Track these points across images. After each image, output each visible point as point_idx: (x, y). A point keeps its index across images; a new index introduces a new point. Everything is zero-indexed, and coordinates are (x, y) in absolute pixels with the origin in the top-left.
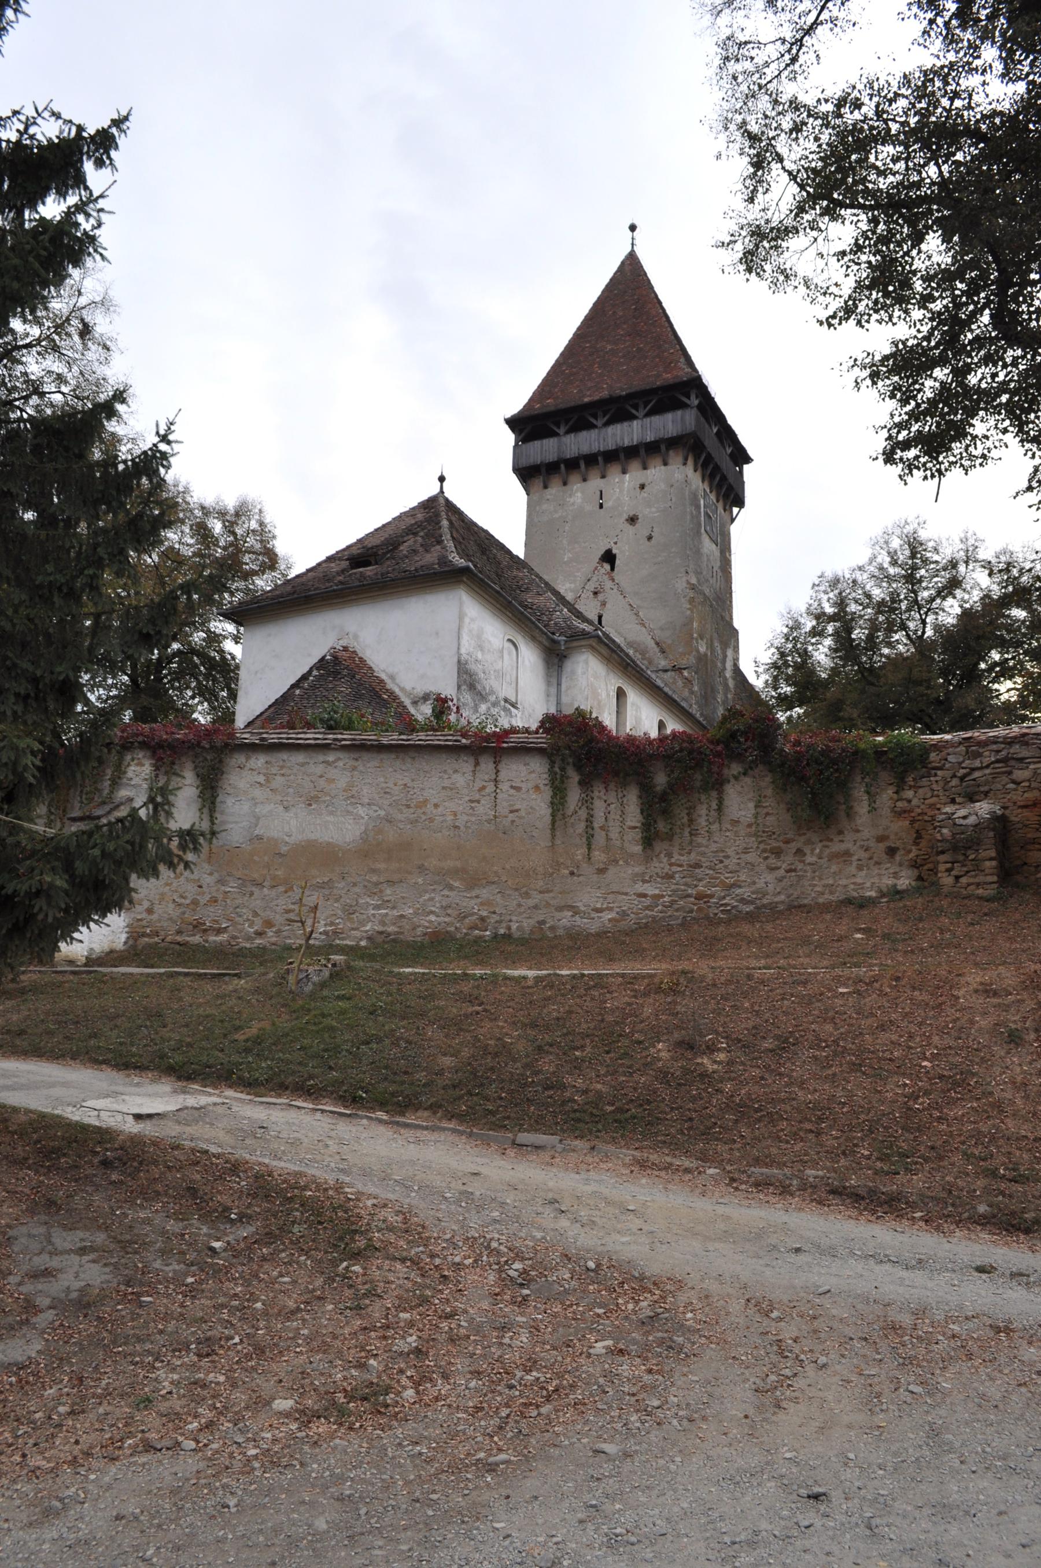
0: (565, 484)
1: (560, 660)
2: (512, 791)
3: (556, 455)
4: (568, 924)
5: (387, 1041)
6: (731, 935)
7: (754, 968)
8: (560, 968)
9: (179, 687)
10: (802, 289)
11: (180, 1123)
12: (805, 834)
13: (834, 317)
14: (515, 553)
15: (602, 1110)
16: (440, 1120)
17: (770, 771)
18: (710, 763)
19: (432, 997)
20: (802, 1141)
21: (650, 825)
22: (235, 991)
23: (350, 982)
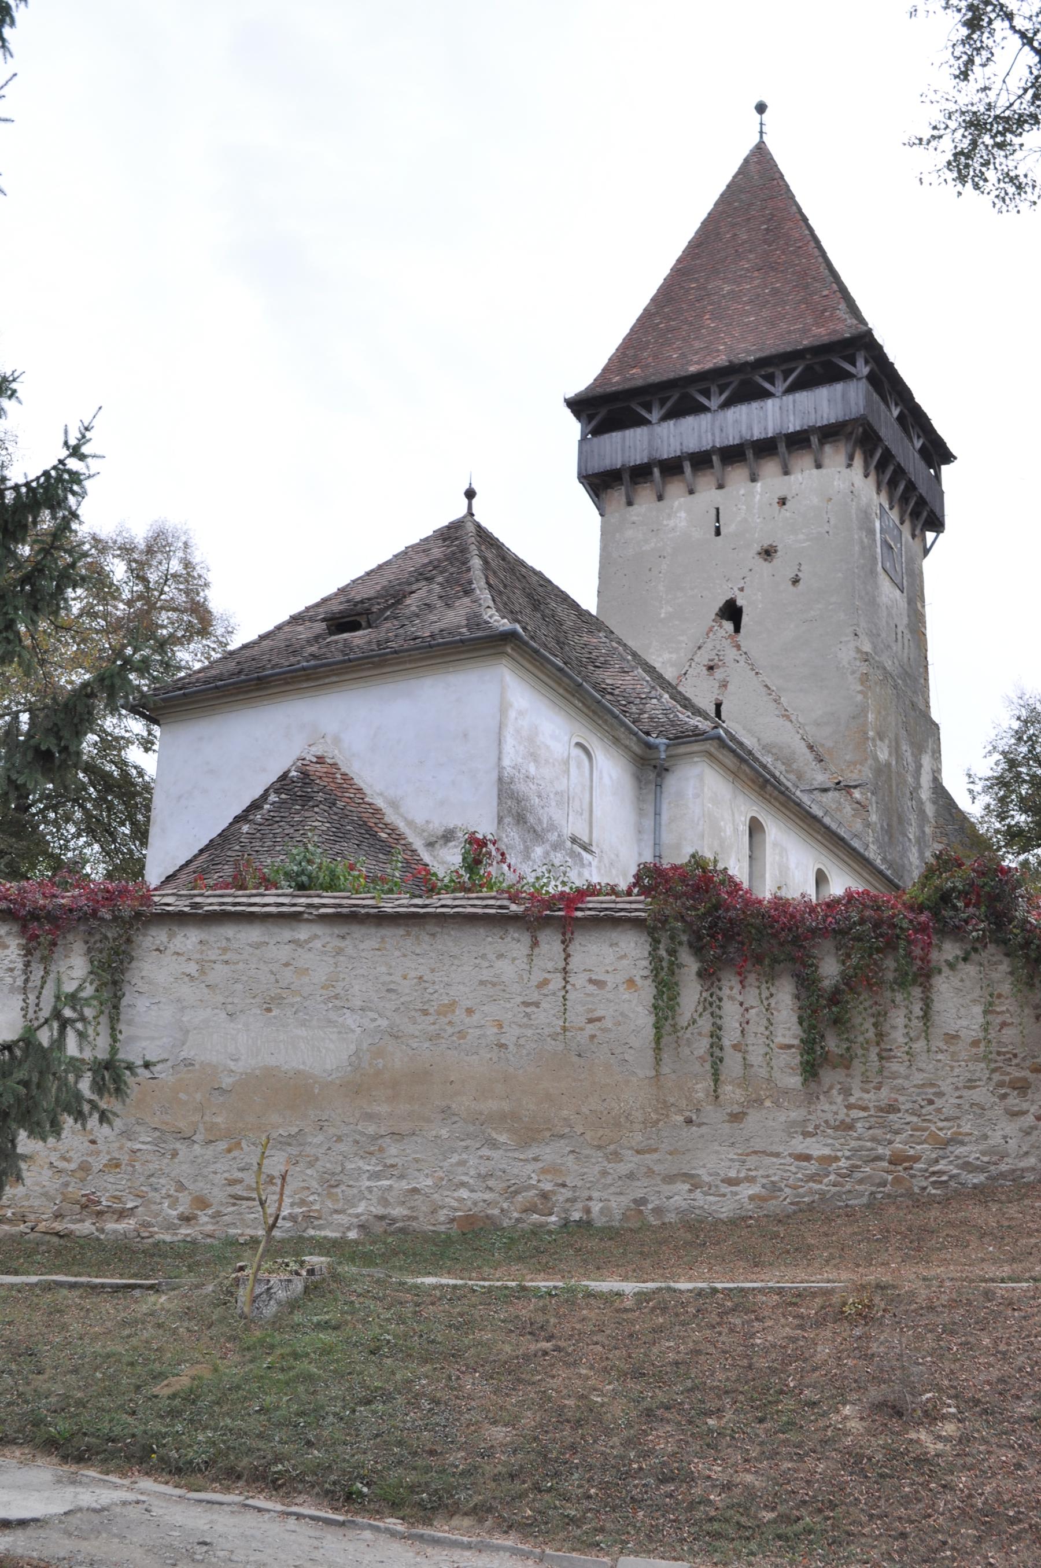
0: (660, 498)
1: (659, 775)
2: (591, 988)
4: (684, 1205)
5: (400, 1400)
6: (950, 1224)
7: (993, 1280)
8: (673, 1277)
9: (56, 820)
11: (70, 1535)
15: (756, 1517)
17: (1007, 955)
18: (910, 942)
19: (468, 1325)
21: (814, 1041)
22: (152, 1314)
23: (336, 1300)
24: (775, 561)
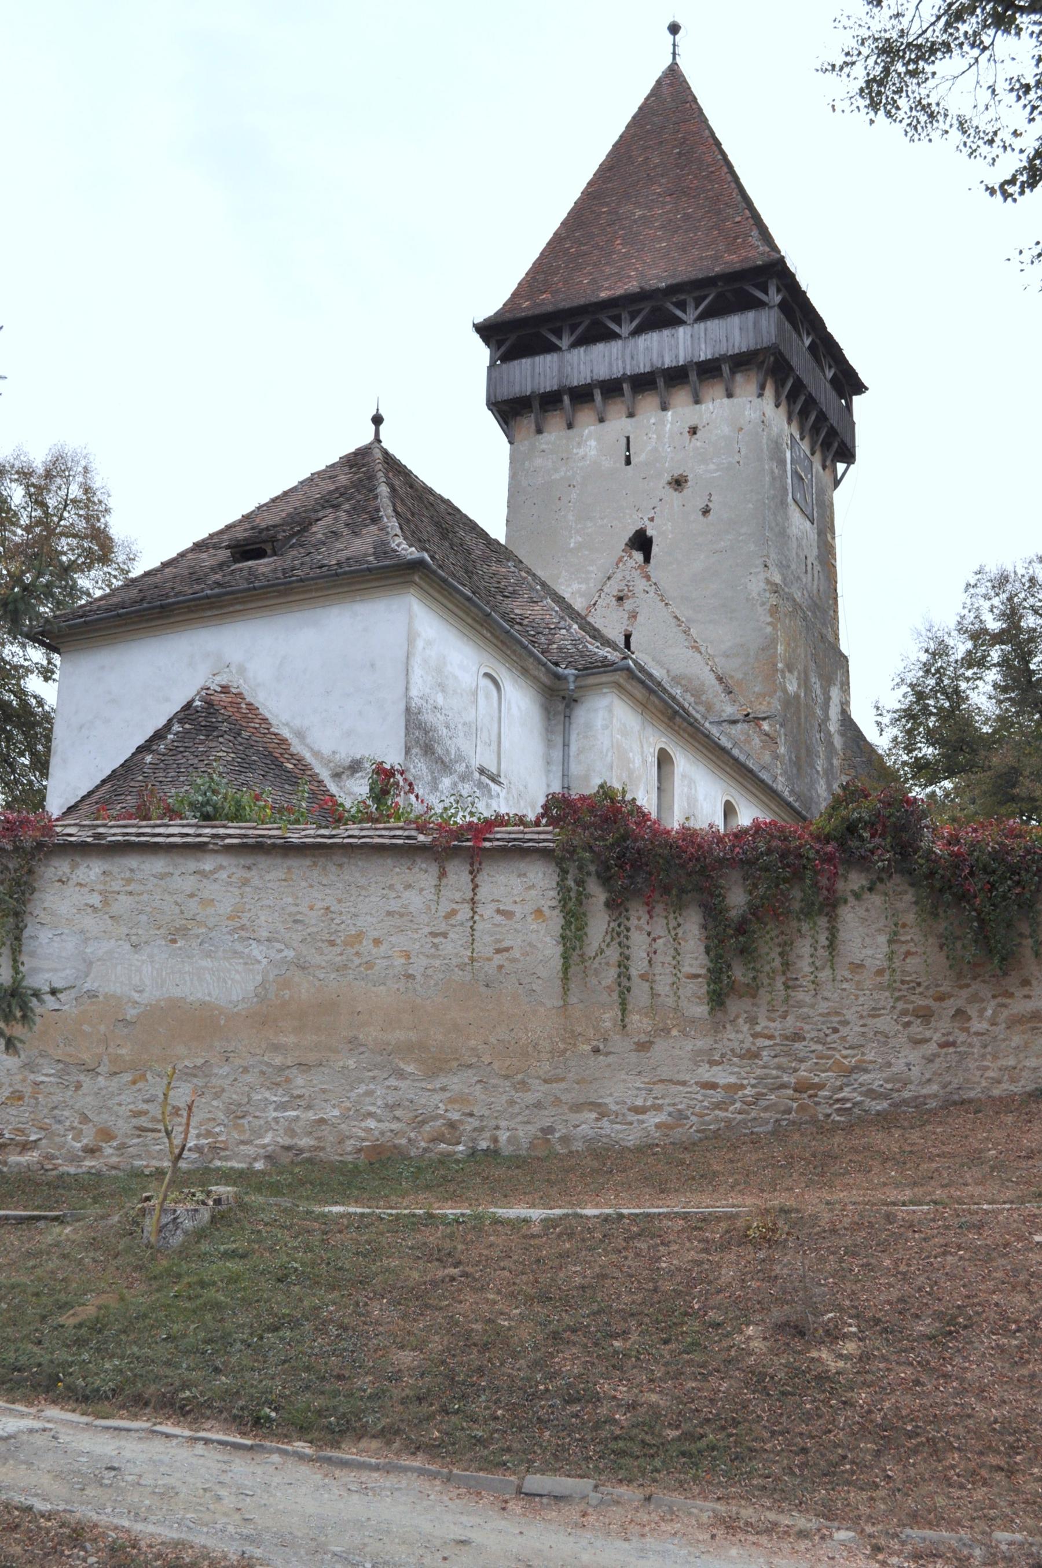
0: (570, 426)
1: (568, 706)
2: (499, 918)
3: (555, 381)
4: (590, 1132)
5: (308, 1326)
6: (854, 1150)
7: (894, 1204)
10: (955, 135)
12: (968, 986)
13: (1012, 181)
14: (493, 536)
15: (660, 1435)
16: (398, 1453)
17: (912, 885)
18: (816, 872)
20: (985, 1484)
22: (57, 1245)
23: (243, 1229)
24: (685, 491)
